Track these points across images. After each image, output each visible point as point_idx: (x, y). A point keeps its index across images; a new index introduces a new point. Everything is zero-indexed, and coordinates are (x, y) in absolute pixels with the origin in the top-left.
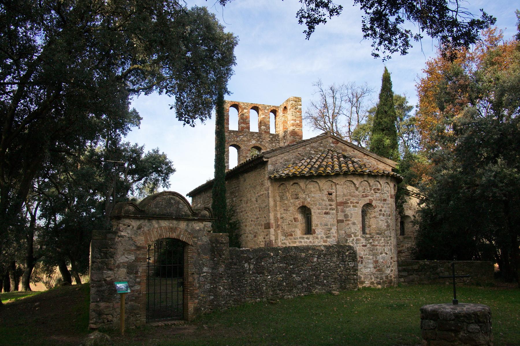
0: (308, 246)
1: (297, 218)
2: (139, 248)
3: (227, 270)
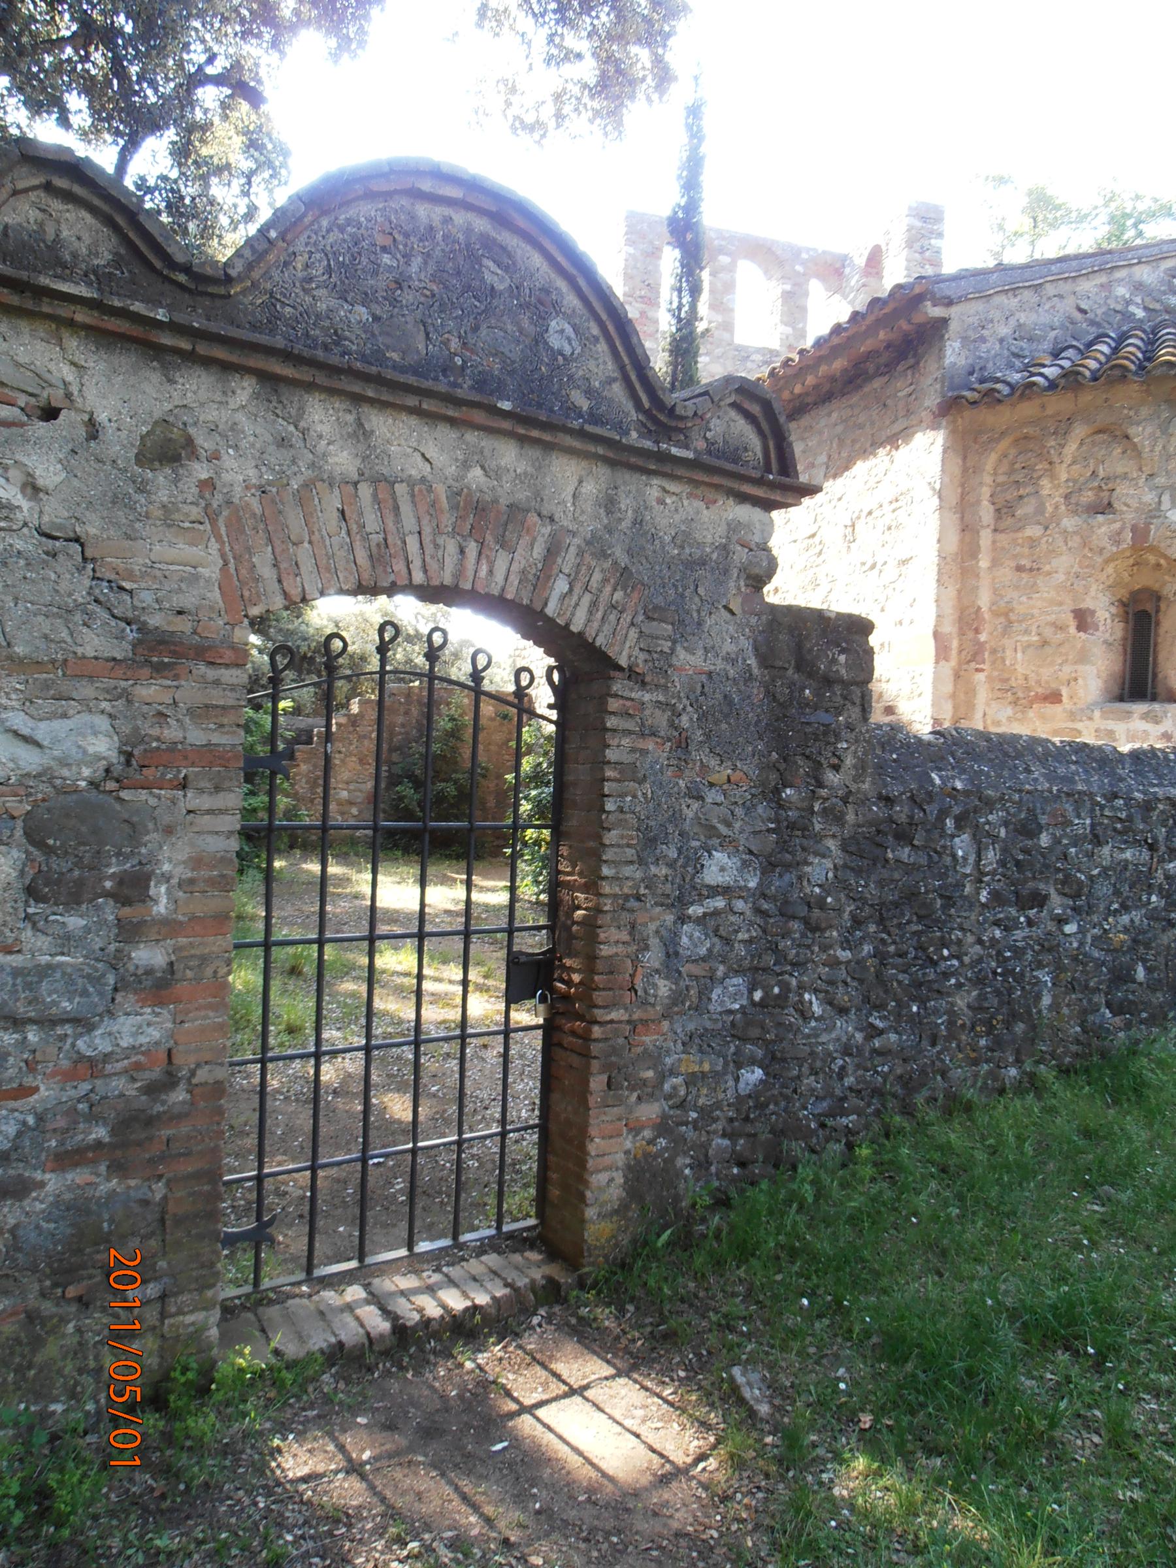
0: (1153, 750)
1: (1093, 612)
2: (160, 652)
3: (858, 872)
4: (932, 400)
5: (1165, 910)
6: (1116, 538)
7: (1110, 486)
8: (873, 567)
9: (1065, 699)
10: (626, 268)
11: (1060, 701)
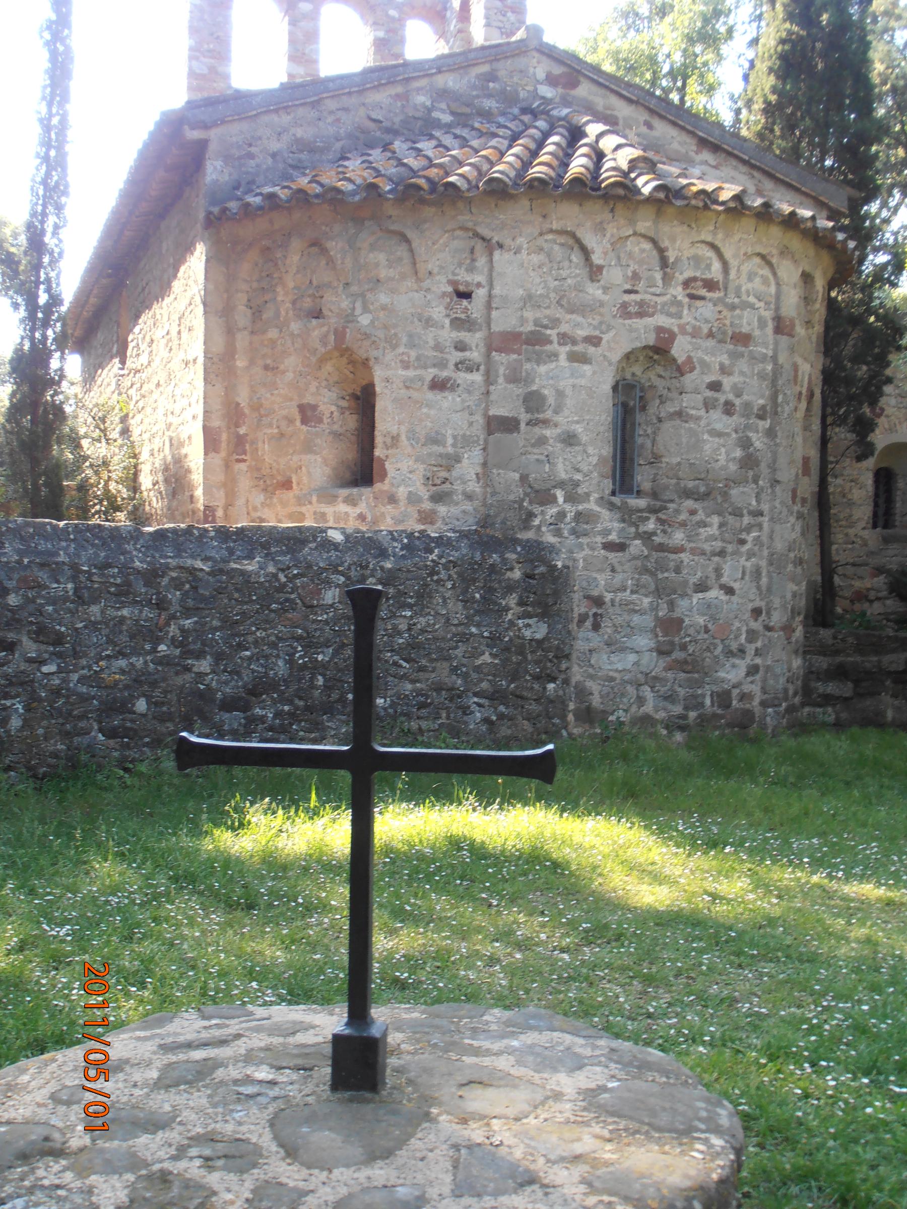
5: (181, 657)
6: (324, 340)
7: (320, 293)
9: (294, 485)
10: (191, 21)
11: (291, 488)
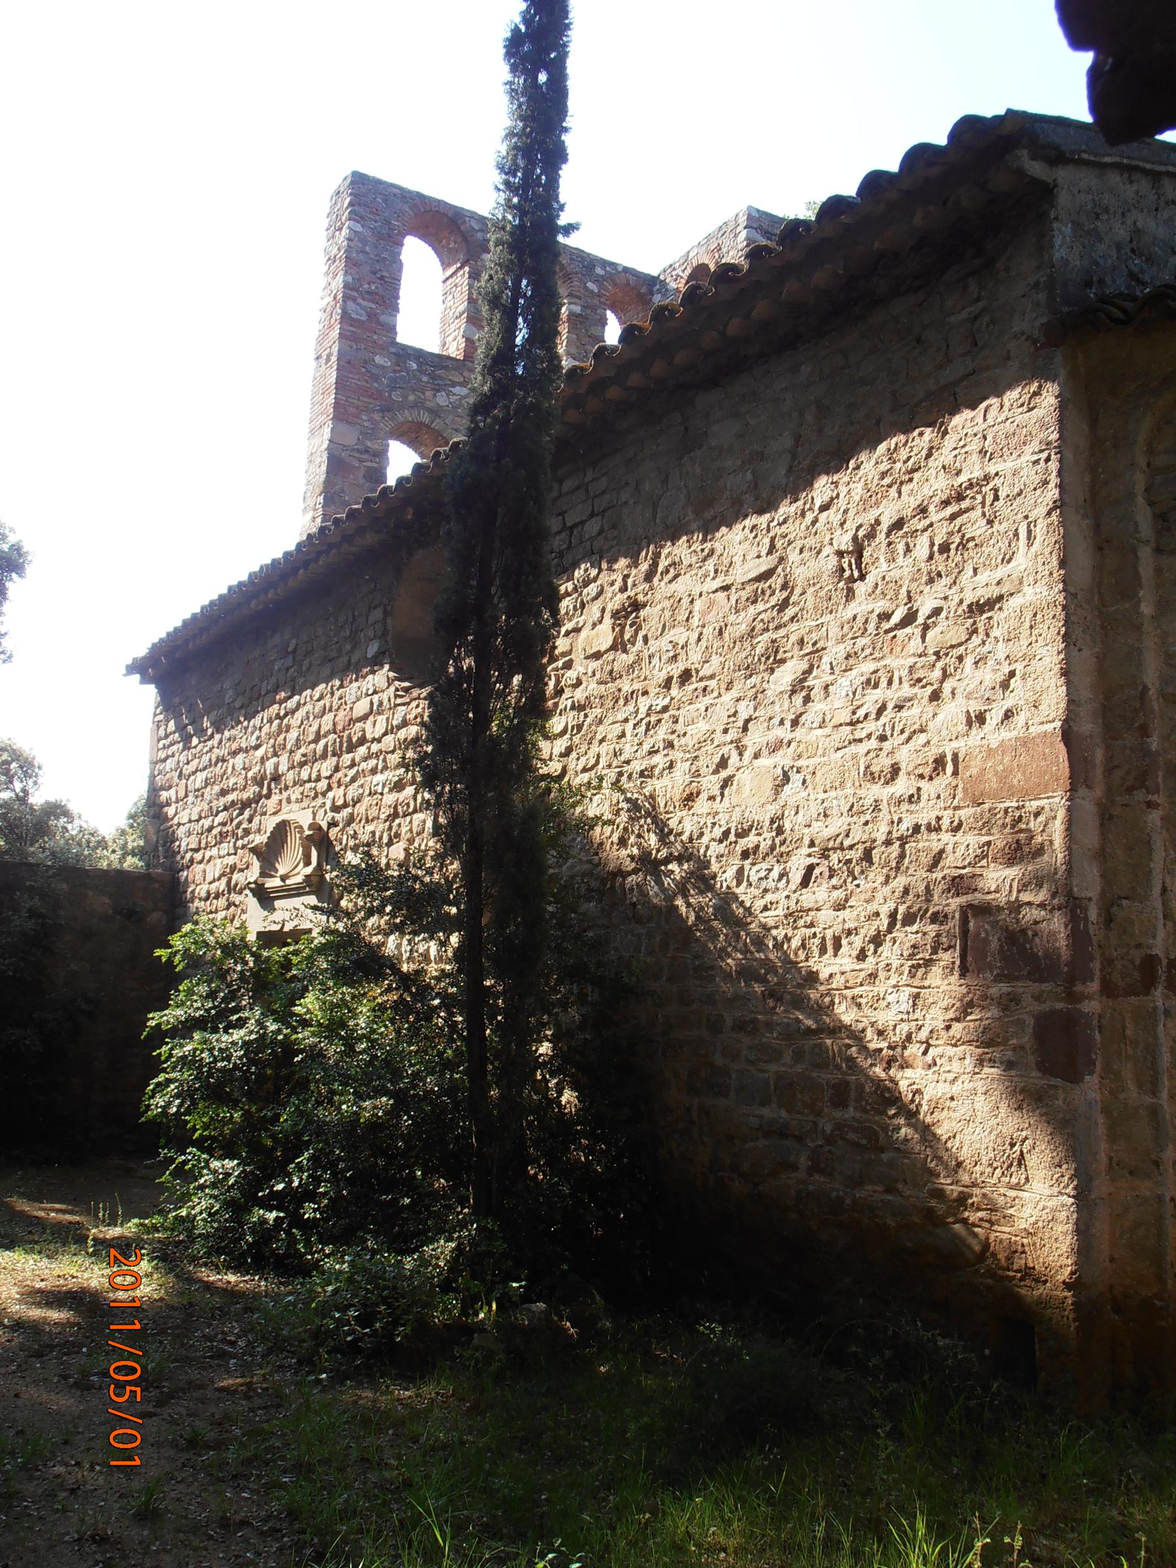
4: (1030, 319)
8: (909, 619)
